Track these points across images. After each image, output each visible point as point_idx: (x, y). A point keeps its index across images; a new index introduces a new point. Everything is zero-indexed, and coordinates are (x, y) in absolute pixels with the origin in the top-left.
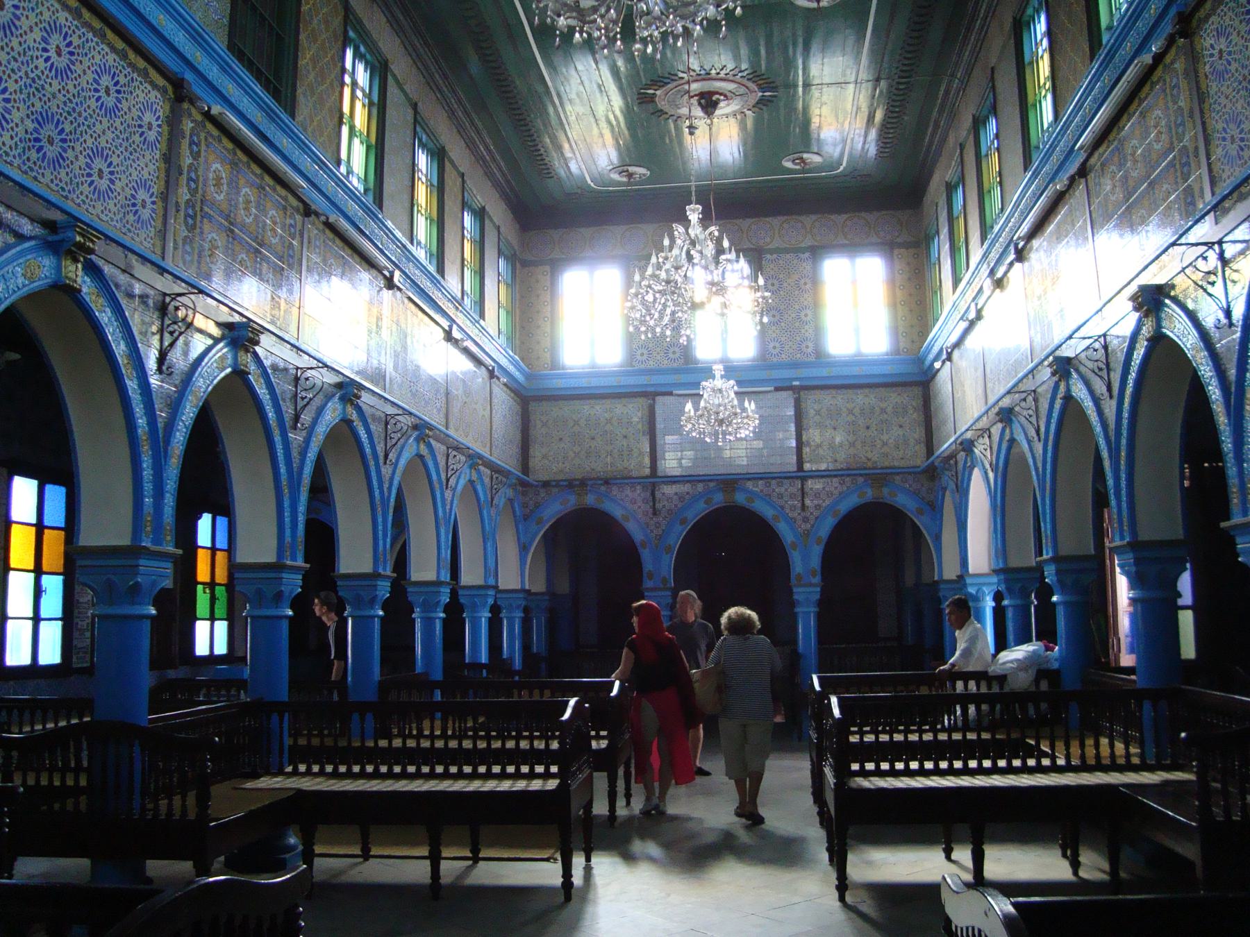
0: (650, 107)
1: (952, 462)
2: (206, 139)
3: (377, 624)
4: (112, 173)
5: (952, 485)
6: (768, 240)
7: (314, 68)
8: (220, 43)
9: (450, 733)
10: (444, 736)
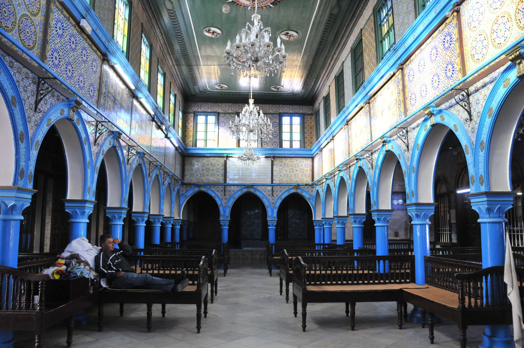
4: (73, 71)
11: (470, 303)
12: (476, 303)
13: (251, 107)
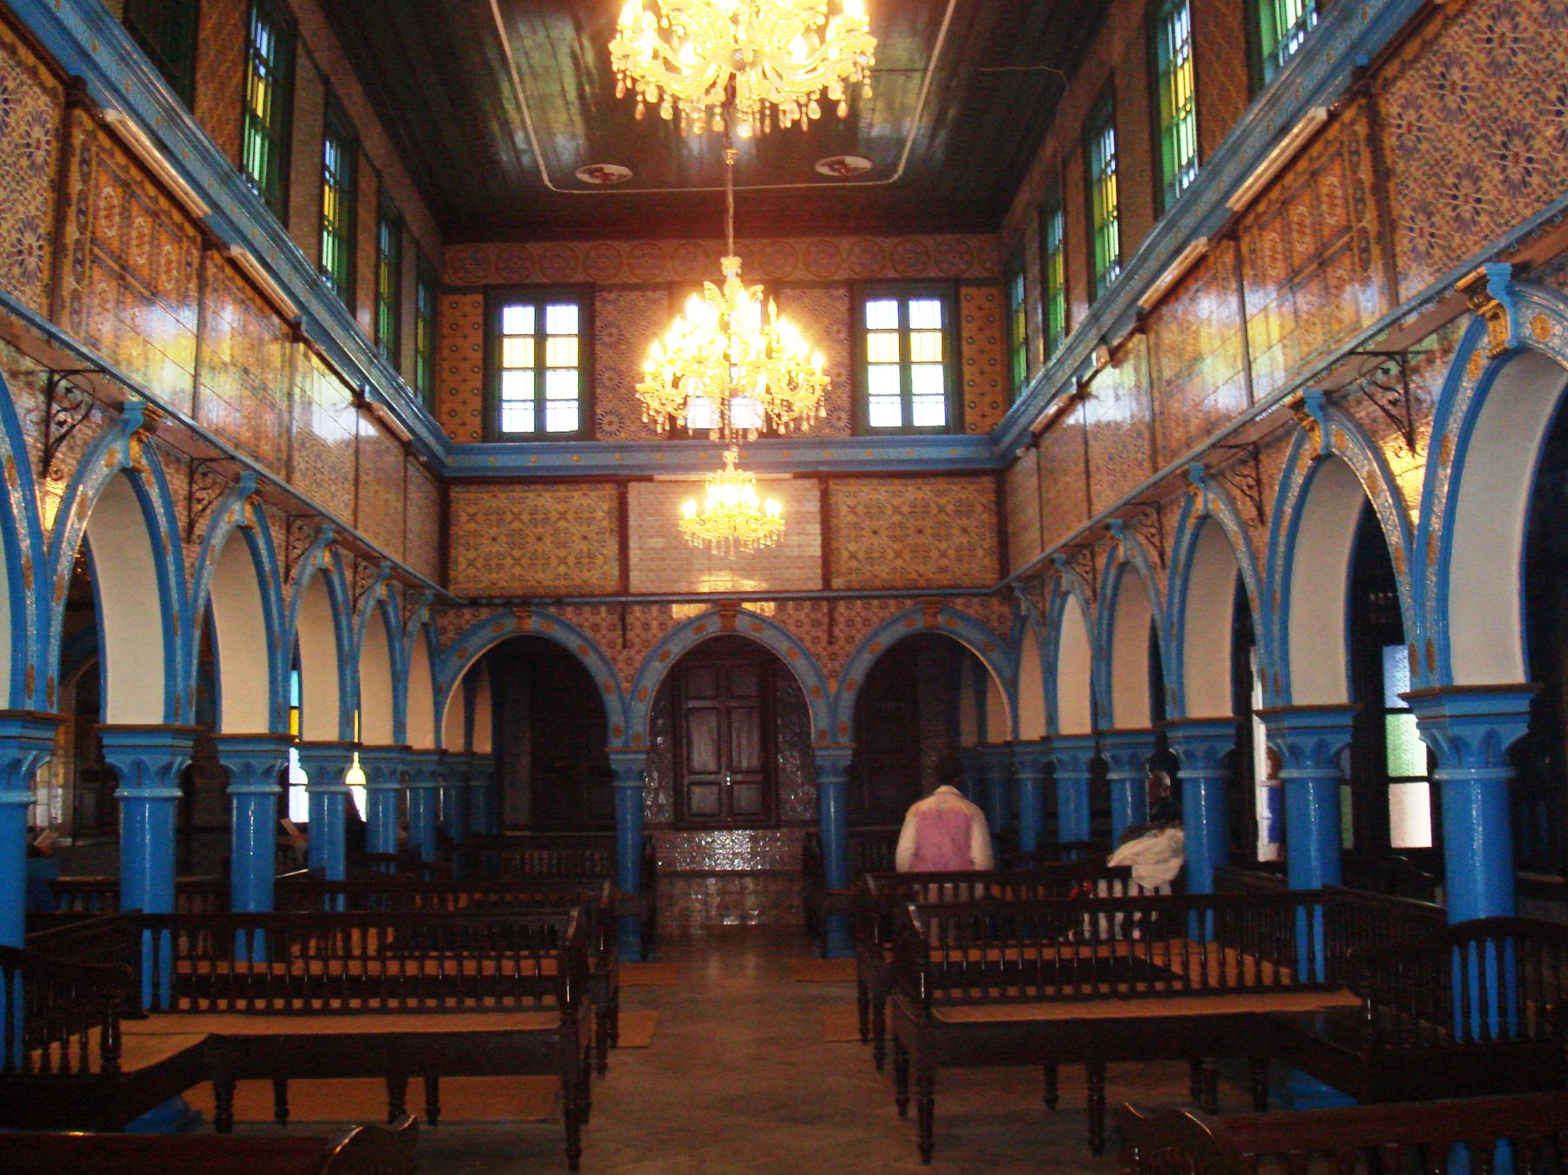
2: (97, 155)
6: (789, 269)
9: (312, 952)
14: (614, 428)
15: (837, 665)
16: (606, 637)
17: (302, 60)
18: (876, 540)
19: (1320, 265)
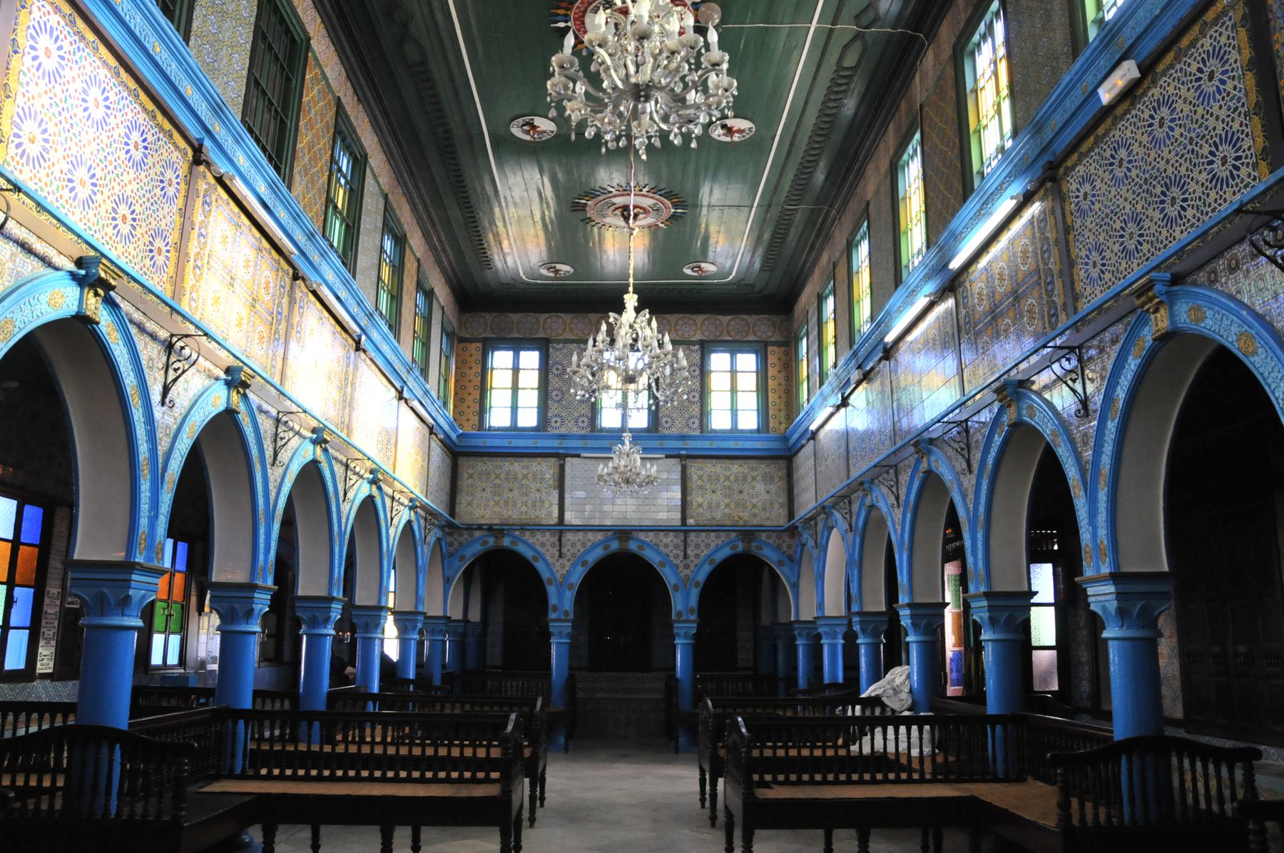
0: (580, 215)
1: (812, 523)
3: (329, 641)
5: (811, 543)
7: (309, 152)
8: (235, 114)
9: (389, 740)
10: (384, 742)
11: (1096, 816)
12: (1109, 817)
13: (630, 317)
14: (558, 424)
15: (689, 572)
16: (550, 553)
17: (369, 179)
18: (714, 496)
19: (1015, 299)
